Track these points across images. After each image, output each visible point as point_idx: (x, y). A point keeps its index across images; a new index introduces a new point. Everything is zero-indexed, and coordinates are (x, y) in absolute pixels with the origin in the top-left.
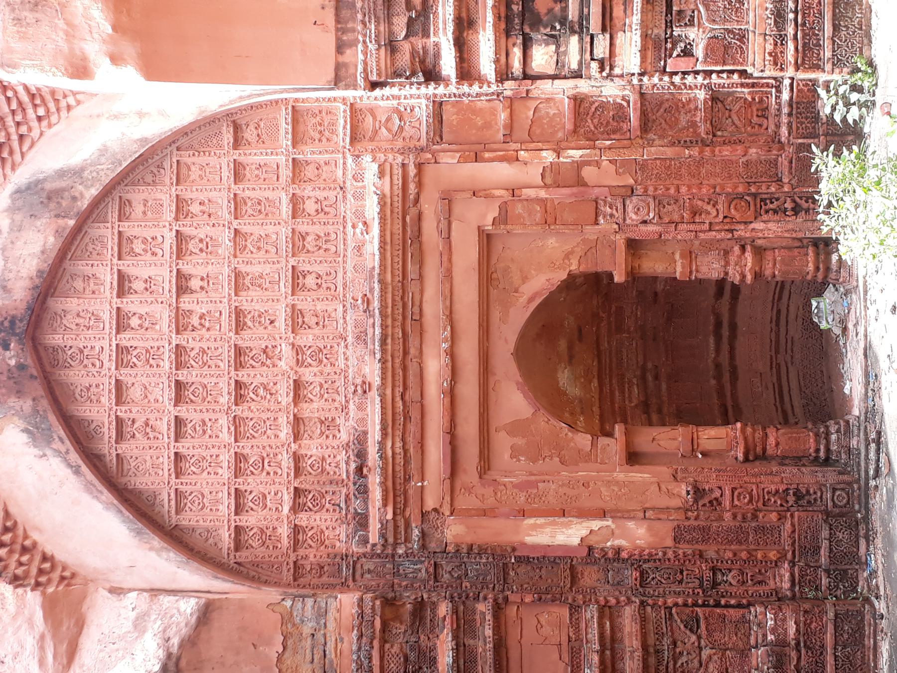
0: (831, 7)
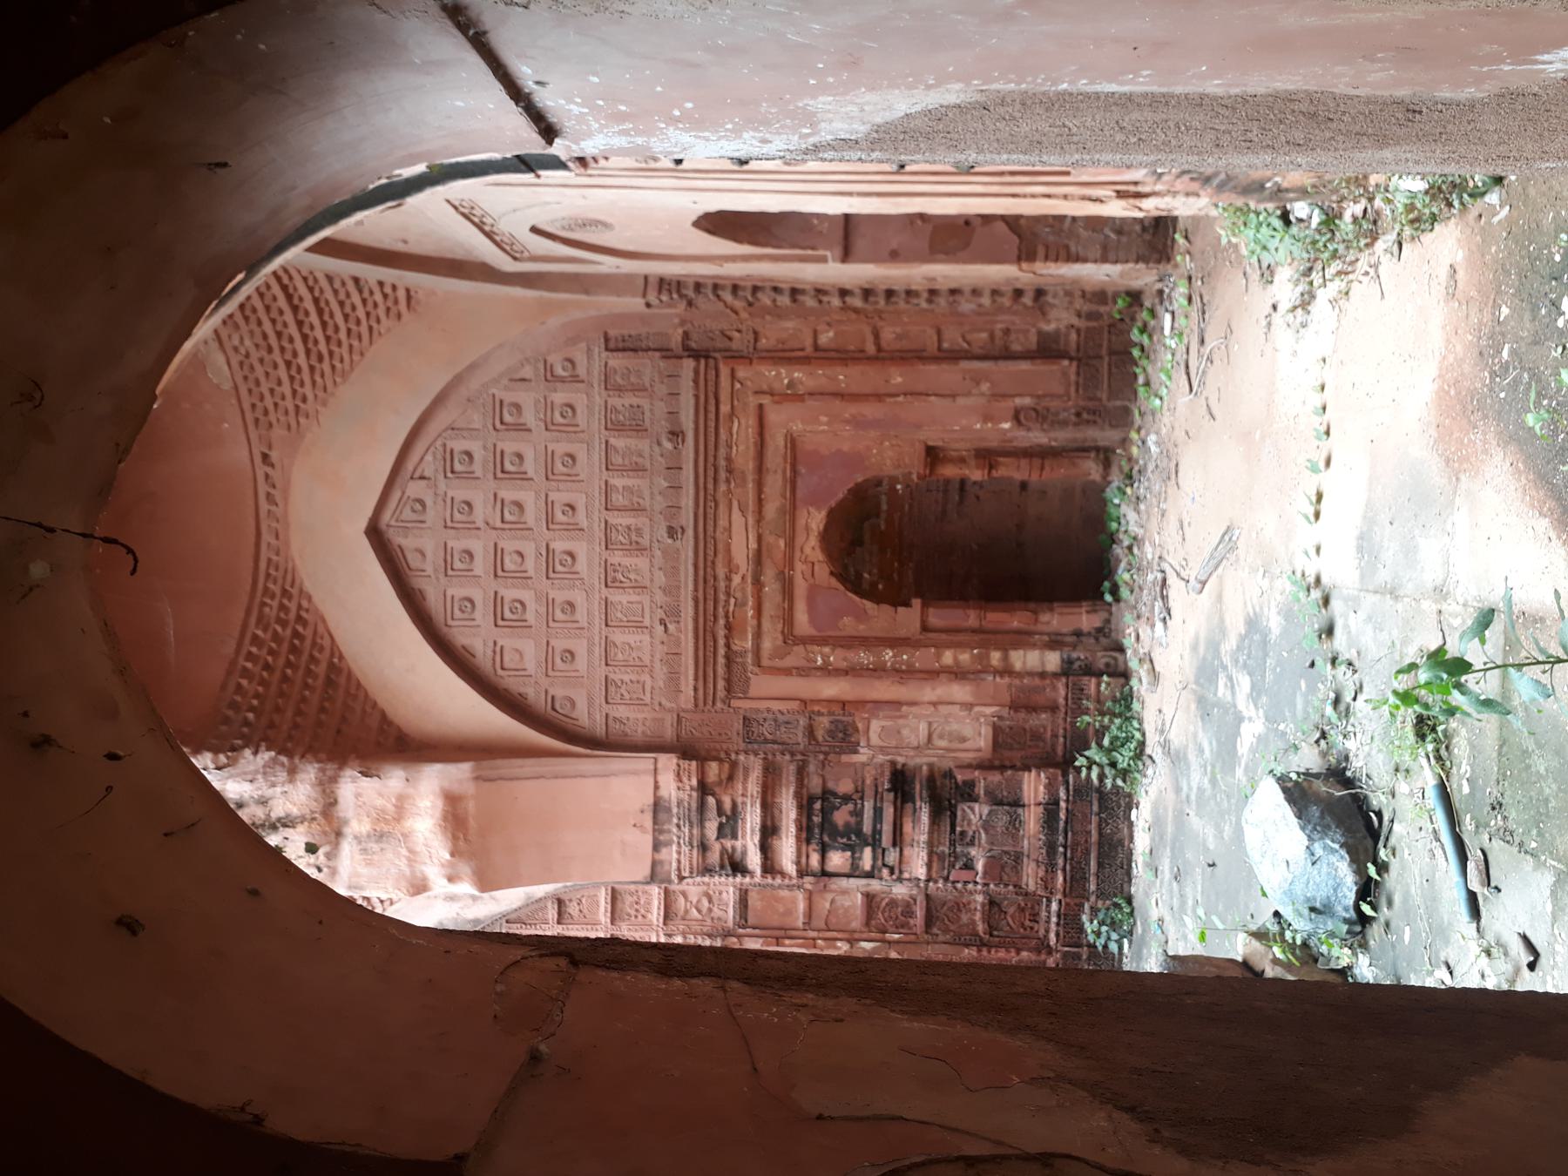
0: (1100, 170)
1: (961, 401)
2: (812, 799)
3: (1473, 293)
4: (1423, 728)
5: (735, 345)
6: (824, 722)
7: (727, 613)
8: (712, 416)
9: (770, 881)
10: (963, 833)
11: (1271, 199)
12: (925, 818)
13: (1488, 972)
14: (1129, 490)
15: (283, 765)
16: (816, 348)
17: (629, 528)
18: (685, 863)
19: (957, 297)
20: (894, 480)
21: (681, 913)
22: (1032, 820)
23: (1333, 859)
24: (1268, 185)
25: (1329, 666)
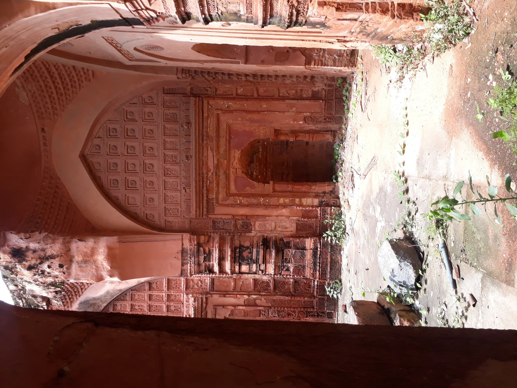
1: (286, 114)
2: (236, 248)
3: (458, 74)
4: (439, 223)
5: (209, 93)
6: (240, 222)
7: (207, 187)
8: (201, 117)
9: (221, 276)
10: (286, 259)
11: (390, 43)
12: (273, 254)
13: (459, 307)
14: (341, 145)
15: (50, 237)
16: (237, 95)
17: (172, 155)
18: (193, 270)
19: (285, 78)
20: (264, 141)
21: (192, 287)
22: (309, 255)
23: (408, 268)
24: (389, 37)
25: (407, 203)
